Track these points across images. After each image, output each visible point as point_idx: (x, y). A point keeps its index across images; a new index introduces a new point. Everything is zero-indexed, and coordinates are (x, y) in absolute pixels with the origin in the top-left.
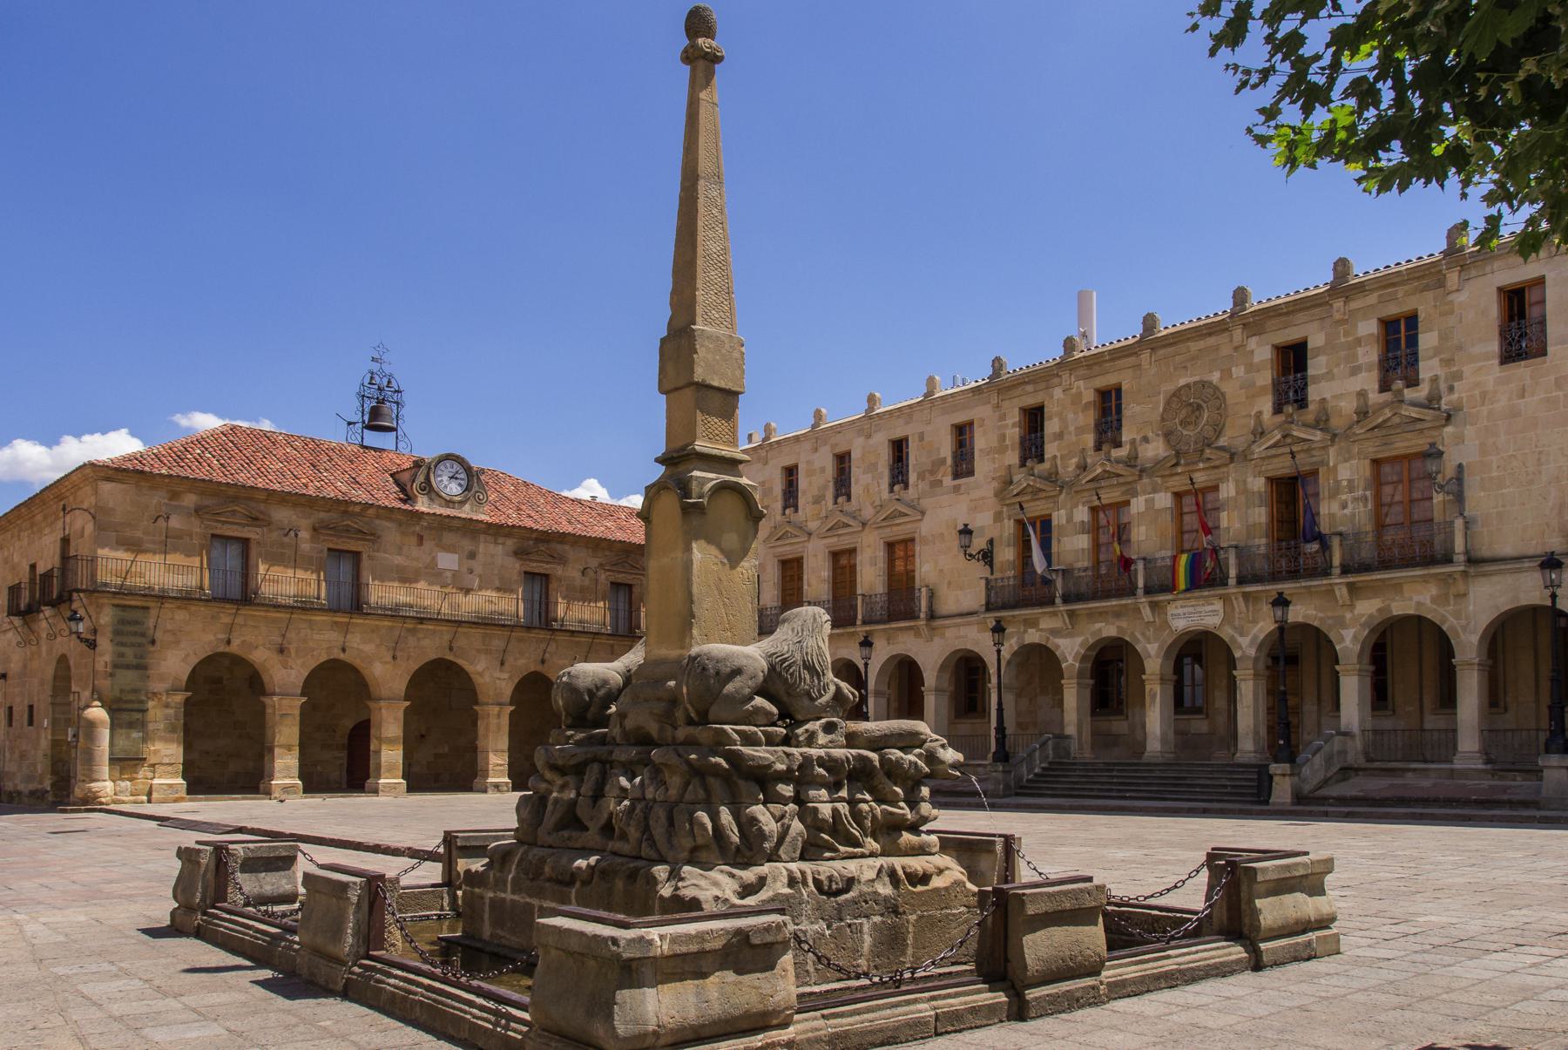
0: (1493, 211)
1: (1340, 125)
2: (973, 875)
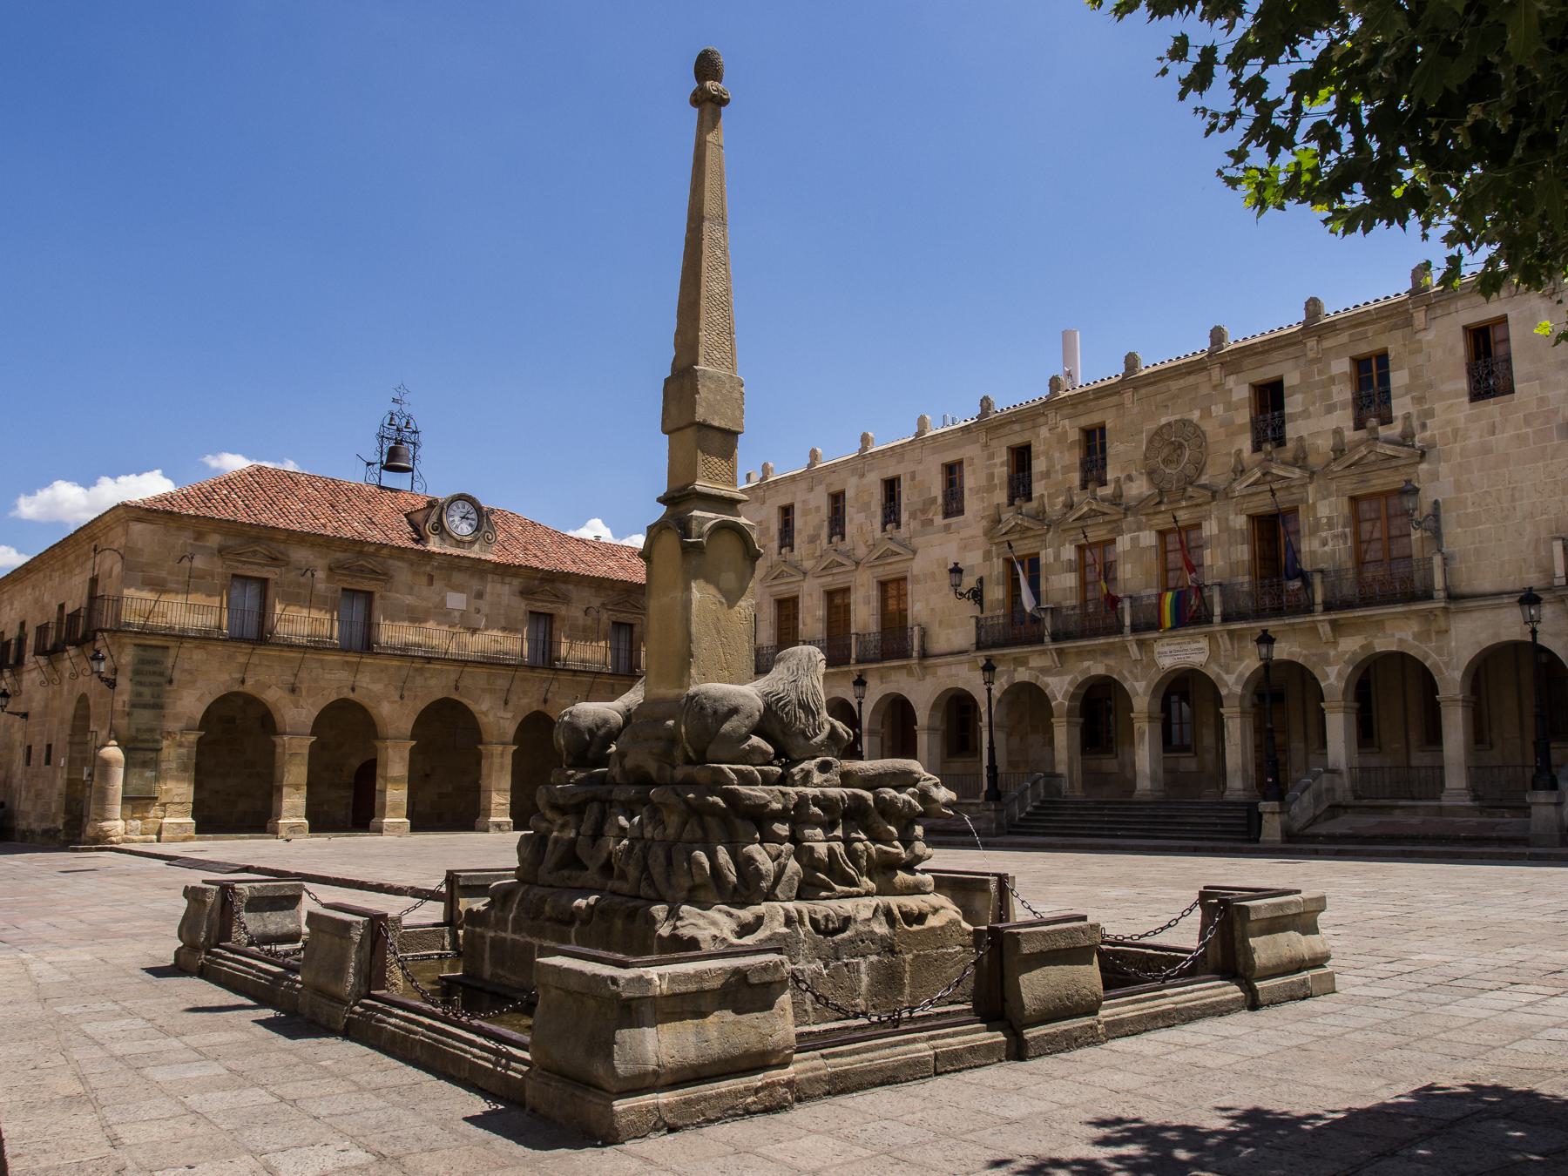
0: (1454, 252)
1: (1304, 167)
2: (967, 916)
